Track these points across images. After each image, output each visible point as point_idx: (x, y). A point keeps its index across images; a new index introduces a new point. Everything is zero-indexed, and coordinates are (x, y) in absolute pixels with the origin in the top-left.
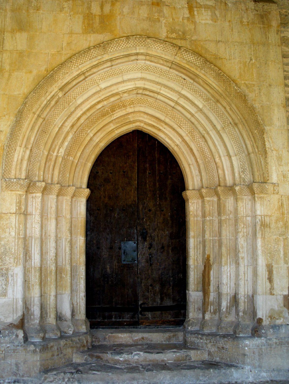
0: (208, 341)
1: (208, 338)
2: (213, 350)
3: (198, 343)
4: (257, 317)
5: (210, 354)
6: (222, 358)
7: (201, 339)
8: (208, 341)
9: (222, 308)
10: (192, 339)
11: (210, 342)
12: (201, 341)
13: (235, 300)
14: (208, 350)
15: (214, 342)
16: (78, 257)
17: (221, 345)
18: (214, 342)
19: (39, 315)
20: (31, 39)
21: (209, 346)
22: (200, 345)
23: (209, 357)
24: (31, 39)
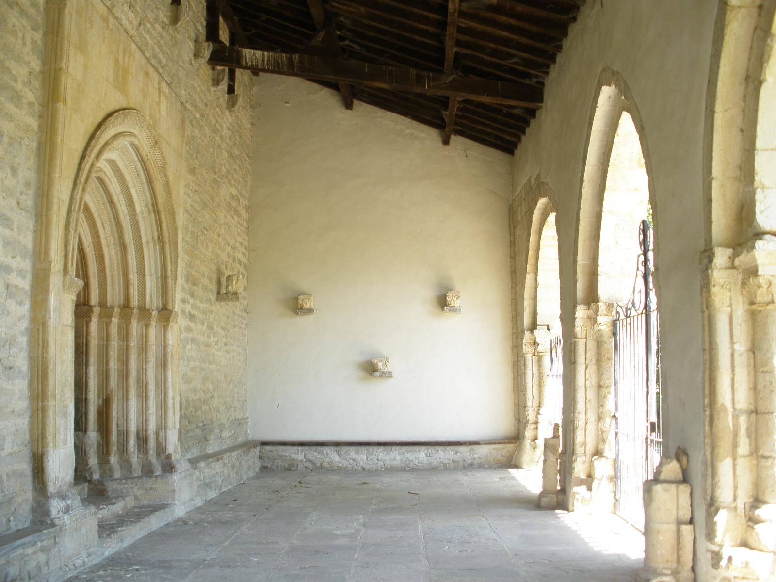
0: (134, 485)
1: (133, 481)
2: (139, 493)
3: (122, 489)
4: (167, 453)
5: (136, 498)
6: (150, 500)
7: (125, 484)
8: (134, 485)
9: (129, 448)
10: (115, 486)
11: (136, 485)
12: (126, 486)
13: (142, 440)
14: (134, 495)
15: (140, 485)
16: (81, 437)
17: (148, 486)
18: (140, 485)
19: (730, 15)
20: (25, 98)
21: (135, 490)
22: (124, 491)
23: (136, 502)
24: (25, 98)
